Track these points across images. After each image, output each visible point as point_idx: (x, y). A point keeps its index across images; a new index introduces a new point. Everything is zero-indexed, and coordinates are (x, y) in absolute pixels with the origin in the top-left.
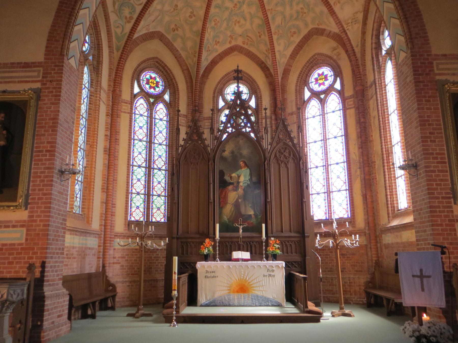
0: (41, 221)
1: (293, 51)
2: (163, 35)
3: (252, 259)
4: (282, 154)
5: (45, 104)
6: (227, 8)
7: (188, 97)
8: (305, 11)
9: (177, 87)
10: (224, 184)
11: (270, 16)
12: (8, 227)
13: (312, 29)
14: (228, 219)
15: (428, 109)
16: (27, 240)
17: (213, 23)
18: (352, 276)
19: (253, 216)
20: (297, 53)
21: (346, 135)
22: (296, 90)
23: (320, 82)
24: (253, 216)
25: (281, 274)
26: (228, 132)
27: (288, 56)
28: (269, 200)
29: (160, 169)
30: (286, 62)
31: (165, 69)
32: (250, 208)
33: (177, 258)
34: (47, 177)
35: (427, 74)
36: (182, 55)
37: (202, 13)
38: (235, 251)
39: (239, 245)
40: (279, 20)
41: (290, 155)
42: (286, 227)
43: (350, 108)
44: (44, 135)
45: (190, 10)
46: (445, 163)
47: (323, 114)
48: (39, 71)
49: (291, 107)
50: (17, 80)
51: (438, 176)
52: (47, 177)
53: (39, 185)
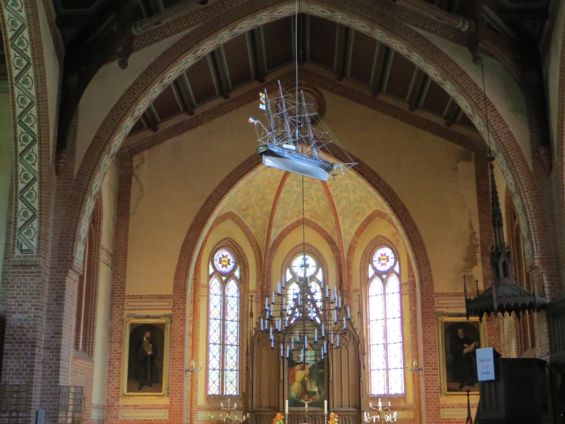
0: (178, 405)
1: (358, 229)
2: (234, 214)
6: (295, 192)
7: (258, 273)
8: (368, 197)
9: (247, 263)
10: (292, 363)
11: (334, 200)
12: (157, 409)
13: (376, 210)
16: (169, 417)
19: (317, 393)
20: (362, 232)
21: (402, 317)
22: (361, 268)
23: (383, 262)
24: (317, 393)
26: (296, 317)
28: (331, 379)
29: (232, 345)
30: (351, 239)
31: (236, 247)
32: (315, 386)
34: (179, 376)
35: (430, 307)
36: (252, 230)
37: (272, 198)
39: (305, 418)
40: (343, 203)
41: (350, 338)
42: (345, 402)
43: (405, 294)
45: (261, 195)
46: (437, 369)
47: (384, 294)
48: (170, 302)
49: (355, 284)
52: (179, 376)
53: (175, 382)
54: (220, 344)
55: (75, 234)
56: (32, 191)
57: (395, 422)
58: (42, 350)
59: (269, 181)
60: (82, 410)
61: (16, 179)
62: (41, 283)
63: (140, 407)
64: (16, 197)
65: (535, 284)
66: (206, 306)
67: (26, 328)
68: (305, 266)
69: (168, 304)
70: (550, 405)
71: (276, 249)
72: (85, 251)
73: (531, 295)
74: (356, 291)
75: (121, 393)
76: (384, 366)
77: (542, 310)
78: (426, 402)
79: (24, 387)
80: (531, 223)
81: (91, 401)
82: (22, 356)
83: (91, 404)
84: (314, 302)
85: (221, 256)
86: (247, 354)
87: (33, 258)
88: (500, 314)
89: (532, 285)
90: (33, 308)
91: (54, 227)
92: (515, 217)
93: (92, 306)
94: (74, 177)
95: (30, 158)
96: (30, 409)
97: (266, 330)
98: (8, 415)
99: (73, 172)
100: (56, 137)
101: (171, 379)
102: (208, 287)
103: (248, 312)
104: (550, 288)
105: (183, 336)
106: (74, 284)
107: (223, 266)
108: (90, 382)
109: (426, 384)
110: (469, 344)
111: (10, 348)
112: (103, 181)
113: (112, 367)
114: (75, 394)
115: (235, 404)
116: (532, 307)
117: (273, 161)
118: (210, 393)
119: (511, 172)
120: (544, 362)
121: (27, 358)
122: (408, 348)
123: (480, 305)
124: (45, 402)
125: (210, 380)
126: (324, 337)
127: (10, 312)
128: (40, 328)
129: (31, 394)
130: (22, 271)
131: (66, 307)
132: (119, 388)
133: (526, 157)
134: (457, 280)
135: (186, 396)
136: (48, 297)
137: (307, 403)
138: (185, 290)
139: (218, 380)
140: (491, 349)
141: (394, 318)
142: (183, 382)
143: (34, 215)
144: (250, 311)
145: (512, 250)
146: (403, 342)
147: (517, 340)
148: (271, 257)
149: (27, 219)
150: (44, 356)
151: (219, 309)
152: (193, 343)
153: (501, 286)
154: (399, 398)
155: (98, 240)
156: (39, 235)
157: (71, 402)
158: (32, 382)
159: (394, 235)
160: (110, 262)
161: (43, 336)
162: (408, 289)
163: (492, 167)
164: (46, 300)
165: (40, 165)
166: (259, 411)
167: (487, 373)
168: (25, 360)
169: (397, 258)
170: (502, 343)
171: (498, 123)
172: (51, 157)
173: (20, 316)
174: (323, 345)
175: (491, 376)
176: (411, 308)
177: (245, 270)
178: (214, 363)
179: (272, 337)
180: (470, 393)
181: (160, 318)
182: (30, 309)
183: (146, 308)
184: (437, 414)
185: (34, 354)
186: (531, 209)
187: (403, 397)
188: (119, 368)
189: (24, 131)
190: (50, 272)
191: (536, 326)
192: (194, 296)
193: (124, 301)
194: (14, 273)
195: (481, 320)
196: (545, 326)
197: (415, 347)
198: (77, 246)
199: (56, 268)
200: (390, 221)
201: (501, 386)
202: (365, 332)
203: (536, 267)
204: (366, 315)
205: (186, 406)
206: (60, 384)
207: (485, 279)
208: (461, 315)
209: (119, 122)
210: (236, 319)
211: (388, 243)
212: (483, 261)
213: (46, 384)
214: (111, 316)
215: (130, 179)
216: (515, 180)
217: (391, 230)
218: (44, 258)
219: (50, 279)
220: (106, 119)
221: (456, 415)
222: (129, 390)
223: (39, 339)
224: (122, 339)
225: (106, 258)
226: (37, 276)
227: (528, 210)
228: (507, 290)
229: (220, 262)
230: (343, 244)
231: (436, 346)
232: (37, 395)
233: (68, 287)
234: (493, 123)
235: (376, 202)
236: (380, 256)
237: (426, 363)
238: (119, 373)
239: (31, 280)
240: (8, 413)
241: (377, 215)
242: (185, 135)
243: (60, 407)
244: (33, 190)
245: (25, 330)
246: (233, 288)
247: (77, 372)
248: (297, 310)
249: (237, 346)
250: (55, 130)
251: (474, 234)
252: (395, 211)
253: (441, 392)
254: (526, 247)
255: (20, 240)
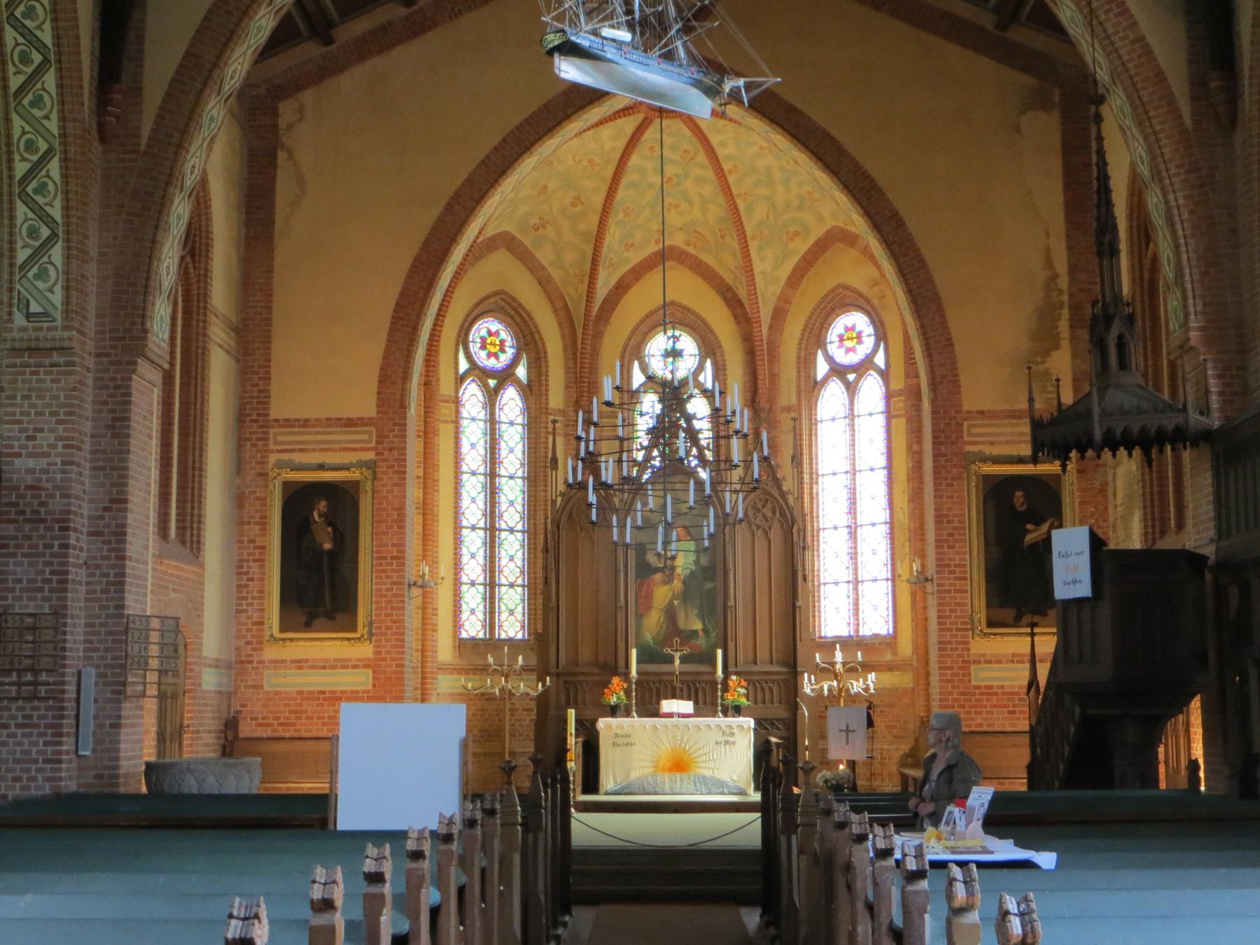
0: (392, 659)
2: (513, 238)
3: (697, 714)
4: (759, 511)
5: (384, 485)
8: (817, 196)
9: (545, 348)
10: (645, 571)
12: (346, 667)
13: (834, 227)
14: (653, 639)
15: (948, 497)
16: (374, 685)
17: (621, 215)
18: (885, 747)
19: (701, 633)
20: (802, 277)
21: (889, 467)
22: (799, 358)
23: (848, 344)
24: (701, 633)
25: (747, 740)
26: (653, 467)
27: (784, 280)
28: (731, 603)
29: (511, 531)
31: (517, 312)
33: (573, 711)
34: (395, 596)
35: (953, 443)
37: (598, 200)
38: (666, 698)
39: (674, 688)
40: (761, 212)
42: (762, 654)
44: (386, 533)
45: (573, 193)
46: (964, 566)
47: (851, 416)
48: (370, 433)
49: (787, 395)
50: (338, 446)
51: (953, 598)
52: (395, 596)
53: (386, 608)
54: (485, 529)
55: (148, 279)
56: (46, 180)
57: (871, 695)
58: (84, 537)
59: (591, 161)
60: (181, 669)
61: (9, 153)
62: (75, 389)
63: (310, 664)
64: (10, 194)
65: (1188, 385)
66: (452, 444)
67: (46, 489)
68: (674, 354)
69: (367, 436)
70: (1212, 654)
71: (609, 318)
72: (174, 318)
73: (1179, 410)
74: (789, 409)
75: (268, 633)
76: (847, 575)
77: (1202, 443)
78: (940, 649)
79: (49, 618)
80: (1183, 248)
81: (201, 651)
82: (41, 550)
83: (200, 657)
84: (693, 435)
85: (484, 333)
86: (546, 550)
87: (55, 333)
88: (1107, 454)
89: (1181, 384)
90: (60, 444)
91: (100, 262)
92: (1148, 239)
93: (194, 442)
94: (143, 147)
95: (38, 102)
96: (64, 666)
97: (579, 483)
98: (14, 678)
99: (138, 136)
100: (97, 54)
101: (376, 602)
102: (457, 402)
103: (546, 457)
104: (1221, 394)
105: (401, 509)
106: (152, 391)
107: (490, 355)
108: (196, 609)
109: (939, 611)
110: (1038, 522)
111: (12, 533)
112: (208, 157)
113: (245, 577)
114: (162, 632)
115: (520, 658)
116: (1179, 437)
117: (579, 68)
118: (464, 635)
119: (1142, 132)
120: (1203, 559)
121: (52, 555)
122: (902, 536)
123: (1059, 435)
124: (96, 650)
125: (464, 607)
126: (709, 497)
127: (8, 455)
128: (76, 489)
129: (65, 633)
130: (32, 361)
131: (135, 443)
132: (262, 623)
133: (1177, 95)
134: (1013, 373)
135: (412, 640)
136: (94, 420)
137: (677, 655)
138: (403, 407)
139: (481, 607)
140: (1085, 530)
141: (872, 470)
142: (403, 609)
143: (54, 235)
144: (550, 455)
145: (1138, 306)
146: (892, 524)
147: (1145, 515)
148: (598, 335)
149: (37, 244)
150: (89, 551)
151: (482, 452)
152: (424, 525)
153: (1110, 390)
154: (880, 644)
155: (205, 295)
156: (68, 281)
157: (154, 650)
158: (65, 607)
159: (875, 283)
160: (233, 343)
161: (85, 505)
162: (902, 404)
163: (1098, 119)
164: (88, 427)
165: (63, 119)
166: (575, 674)
167: (1075, 582)
168: (47, 559)
169: (881, 335)
170: (1111, 520)
171: (1116, 15)
172: (86, 100)
173: (31, 463)
174: (707, 516)
175: (1084, 589)
176: (909, 448)
177: (538, 364)
178: (473, 569)
179: (592, 498)
180: (1036, 630)
181: (348, 469)
182: (53, 446)
183: (318, 447)
184: (964, 675)
185: (66, 546)
186: (1185, 216)
187: (890, 642)
188: (262, 579)
189: (21, 40)
190: (95, 363)
191: (1187, 481)
192: (425, 422)
193: (267, 433)
194: (15, 366)
195: (1064, 467)
196: (1207, 480)
197: (918, 533)
198: (153, 304)
199: (108, 355)
200: (866, 251)
201: (1105, 610)
202: (807, 500)
203: (1192, 348)
204: (811, 464)
205: (411, 661)
206: (126, 612)
207: (1076, 380)
208: (1020, 460)
209: (241, 20)
210: (520, 473)
211: (861, 302)
212: (1073, 338)
213: (97, 611)
214: (239, 465)
215: (274, 156)
216: (1150, 152)
217: (869, 271)
218: (80, 332)
219: (96, 379)
220: (210, 11)
221: (1003, 679)
222: (283, 629)
223: (76, 514)
224: (265, 517)
225: (223, 335)
226: (65, 373)
227: (1177, 219)
228: (1125, 398)
229: (483, 347)
230: (760, 304)
231: (964, 535)
232: (76, 636)
233: (136, 397)
234: (1103, 17)
235: (835, 208)
236: (842, 331)
237: (941, 565)
238: (261, 591)
239: (52, 381)
240: (15, 674)
241: (835, 238)
242: (397, 51)
243: (129, 661)
244: (48, 176)
245: (43, 494)
246: (512, 404)
247: (166, 588)
248: (655, 453)
249: (523, 532)
250: (93, 39)
251: (1055, 277)
252: (877, 226)
253: (972, 629)
254: (1170, 304)
255: (23, 292)
